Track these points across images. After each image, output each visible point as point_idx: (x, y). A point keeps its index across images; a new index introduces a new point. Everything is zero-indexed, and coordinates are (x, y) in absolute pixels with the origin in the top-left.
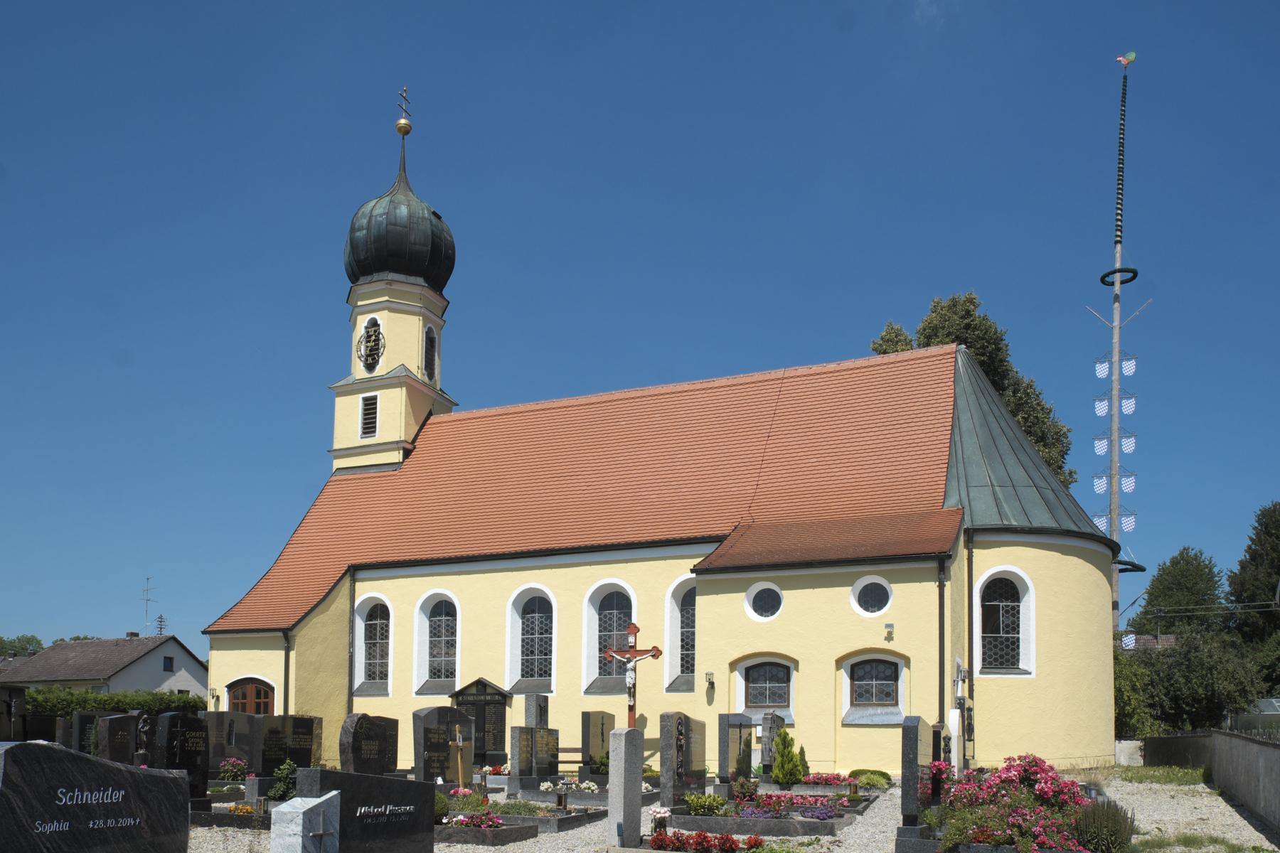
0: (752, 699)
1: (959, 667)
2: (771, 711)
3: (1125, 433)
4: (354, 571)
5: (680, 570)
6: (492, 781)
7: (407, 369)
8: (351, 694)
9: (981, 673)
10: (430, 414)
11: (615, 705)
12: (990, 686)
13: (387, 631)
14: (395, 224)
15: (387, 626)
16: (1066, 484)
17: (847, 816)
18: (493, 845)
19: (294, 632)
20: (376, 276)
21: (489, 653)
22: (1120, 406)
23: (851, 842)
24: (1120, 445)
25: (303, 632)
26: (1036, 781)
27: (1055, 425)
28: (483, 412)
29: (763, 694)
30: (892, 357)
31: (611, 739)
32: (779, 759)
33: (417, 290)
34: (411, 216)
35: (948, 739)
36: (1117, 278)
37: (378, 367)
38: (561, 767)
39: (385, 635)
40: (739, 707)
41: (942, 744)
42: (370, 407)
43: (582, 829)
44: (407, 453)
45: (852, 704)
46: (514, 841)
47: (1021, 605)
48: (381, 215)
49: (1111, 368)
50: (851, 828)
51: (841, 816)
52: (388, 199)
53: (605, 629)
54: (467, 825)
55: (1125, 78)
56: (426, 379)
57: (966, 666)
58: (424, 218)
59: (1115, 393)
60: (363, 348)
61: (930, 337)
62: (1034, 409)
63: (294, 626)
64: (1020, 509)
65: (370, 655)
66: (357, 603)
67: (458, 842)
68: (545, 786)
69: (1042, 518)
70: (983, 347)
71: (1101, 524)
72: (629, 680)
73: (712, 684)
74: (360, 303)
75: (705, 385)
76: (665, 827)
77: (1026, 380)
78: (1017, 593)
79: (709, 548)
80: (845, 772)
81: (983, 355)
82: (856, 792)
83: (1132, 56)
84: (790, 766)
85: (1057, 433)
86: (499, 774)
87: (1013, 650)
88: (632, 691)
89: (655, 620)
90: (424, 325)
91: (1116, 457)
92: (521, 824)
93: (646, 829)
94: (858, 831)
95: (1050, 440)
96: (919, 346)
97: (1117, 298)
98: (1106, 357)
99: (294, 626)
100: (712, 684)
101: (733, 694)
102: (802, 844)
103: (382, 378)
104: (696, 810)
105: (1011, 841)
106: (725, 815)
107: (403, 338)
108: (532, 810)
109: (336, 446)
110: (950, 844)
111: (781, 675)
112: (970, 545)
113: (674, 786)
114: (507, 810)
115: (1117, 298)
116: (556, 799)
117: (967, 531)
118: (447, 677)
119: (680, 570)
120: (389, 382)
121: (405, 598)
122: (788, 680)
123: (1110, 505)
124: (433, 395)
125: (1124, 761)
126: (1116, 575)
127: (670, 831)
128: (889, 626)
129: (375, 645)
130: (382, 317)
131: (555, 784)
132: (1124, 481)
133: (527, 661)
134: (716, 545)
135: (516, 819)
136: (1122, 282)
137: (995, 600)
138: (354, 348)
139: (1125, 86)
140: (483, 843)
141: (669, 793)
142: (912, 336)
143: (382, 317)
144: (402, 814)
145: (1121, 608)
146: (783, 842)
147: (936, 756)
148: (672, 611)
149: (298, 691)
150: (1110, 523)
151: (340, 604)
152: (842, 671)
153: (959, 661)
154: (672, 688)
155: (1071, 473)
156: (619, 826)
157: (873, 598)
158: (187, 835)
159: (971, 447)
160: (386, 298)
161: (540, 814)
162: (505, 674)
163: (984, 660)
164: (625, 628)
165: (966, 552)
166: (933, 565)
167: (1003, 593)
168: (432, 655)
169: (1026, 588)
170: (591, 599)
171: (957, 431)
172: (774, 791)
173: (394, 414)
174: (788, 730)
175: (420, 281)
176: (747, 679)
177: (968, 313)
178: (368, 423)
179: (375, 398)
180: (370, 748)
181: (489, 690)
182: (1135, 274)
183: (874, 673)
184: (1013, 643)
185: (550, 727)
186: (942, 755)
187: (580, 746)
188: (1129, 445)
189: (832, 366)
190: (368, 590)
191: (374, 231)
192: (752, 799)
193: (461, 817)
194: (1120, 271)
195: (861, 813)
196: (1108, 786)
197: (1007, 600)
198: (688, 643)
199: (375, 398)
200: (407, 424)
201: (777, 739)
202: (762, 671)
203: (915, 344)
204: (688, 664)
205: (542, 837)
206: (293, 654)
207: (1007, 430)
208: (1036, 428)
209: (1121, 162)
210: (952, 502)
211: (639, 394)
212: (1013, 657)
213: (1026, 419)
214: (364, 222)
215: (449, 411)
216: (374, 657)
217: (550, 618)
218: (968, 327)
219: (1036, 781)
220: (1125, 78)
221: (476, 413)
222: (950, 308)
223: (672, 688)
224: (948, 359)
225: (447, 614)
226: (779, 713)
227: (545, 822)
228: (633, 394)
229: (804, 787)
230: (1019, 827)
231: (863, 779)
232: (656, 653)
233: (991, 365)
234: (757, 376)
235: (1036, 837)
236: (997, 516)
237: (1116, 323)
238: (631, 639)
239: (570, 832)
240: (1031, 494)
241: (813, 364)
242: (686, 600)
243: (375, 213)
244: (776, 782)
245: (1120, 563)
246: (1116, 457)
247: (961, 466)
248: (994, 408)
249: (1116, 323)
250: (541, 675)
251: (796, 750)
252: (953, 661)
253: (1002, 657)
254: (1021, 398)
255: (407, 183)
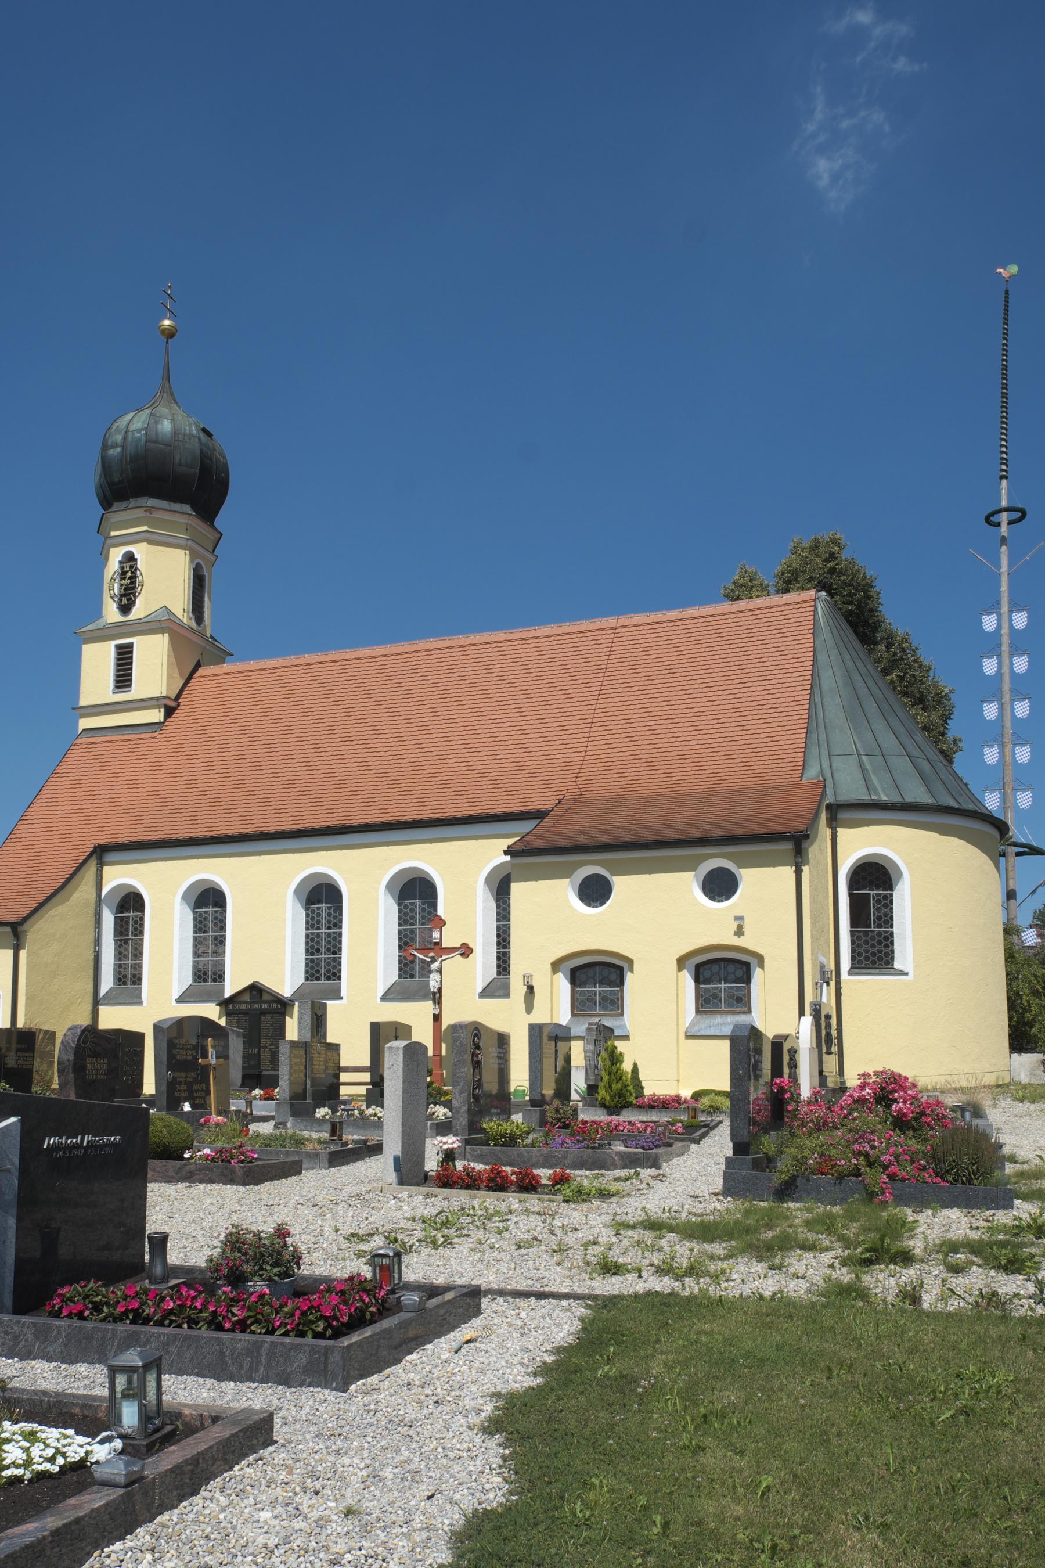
0: (579, 1006)
1: (822, 967)
2: (597, 1020)
3: (1018, 694)
4: (102, 853)
5: (491, 852)
6: (261, 1107)
7: (169, 612)
8: (96, 1003)
9: (850, 973)
10: (198, 665)
11: (417, 1017)
12: (862, 991)
13: (142, 925)
14: (156, 442)
15: (142, 919)
16: (948, 757)
17: (678, 1145)
18: (244, 1184)
19: (25, 927)
20: (133, 502)
21: (266, 952)
22: (1011, 664)
23: (677, 1175)
24: (1013, 709)
25: (36, 927)
26: (895, 1101)
27: (935, 684)
28: (263, 663)
29: (591, 1000)
30: (742, 605)
31: (386, 1054)
32: (606, 1078)
33: (182, 519)
34: (175, 432)
35: (793, 1052)
36: (1004, 517)
37: (134, 609)
38: (344, 1090)
39: (139, 931)
40: (564, 1017)
41: (786, 1058)
42: (124, 656)
43: (359, 1164)
44: (169, 712)
45: (697, 1012)
46: (271, 1179)
47: (896, 894)
48: (139, 431)
49: (999, 621)
50: (681, 1159)
51: (670, 1145)
52: (148, 411)
53: (406, 922)
54: (213, 1160)
55: (1007, 292)
56: (194, 624)
57: (832, 967)
58: (191, 435)
59: (1005, 648)
60: (116, 586)
61: (789, 582)
62: (910, 667)
63: (26, 919)
64: (890, 781)
65: (120, 955)
66: (105, 891)
67: (201, 1181)
68: (322, 1112)
69: (917, 794)
70: (850, 595)
71: (992, 802)
72: (433, 983)
73: (531, 989)
74: (113, 534)
75: (525, 635)
76: (453, 1160)
77: (901, 633)
78: (890, 879)
79: (526, 826)
80: (686, 1093)
81: (850, 603)
82: (695, 1117)
83: (1014, 269)
84: (619, 1086)
85: (937, 694)
86: (270, 1098)
87: (887, 946)
88: (437, 998)
89: (464, 910)
90: (192, 561)
91: (1008, 723)
92: (282, 1158)
93: (432, 1164)
94: (689, 1163)
95: (930, 702)
96: (778, 592)
97: (1003, 540)
98: (994, 608)
99: (26, 919)
100: (531, 989)
101: (556, 1003)
102: (618, 1179)
103: (138, 622)
104: (495, 1139)
105: (856, 1172)
106: (533, 1145)
107: (165, 575)
108: (299, 1142)
109: (83, 702)
110: (785, 1177)
111: (614, 977)
112: (833, 823)
113: (469, 1111)
114: (268, 1141)
115: (1003, 540)
116: (328, 1127)
117: (829, 807)
118: (215, 980)
119: (491, 852)
120: (147, 627)
121: (163, 886)
122: (621, 983)
123: (1005, 778)
124: (202, 643)
125: (1024, 1078)
126: (1012, 859)
127: (459, 1165)
128: (738, 918)
129: (126, 942)
130: (140, 551)
131: (334, 1110)
132: (1018, 750)
133: (312, 961)
134: (536, 822)
135: (278, 1153)
136: (1010, 523)
137: (863, 888)
138: (106, 587)
139: (1007, 301)
140: (232, 1181)
141: (463, 1121)
142: (770, 581)
143: (140, 551)
144: (105, 1145)
145: (1020, 897)
146: (596, 1177)
147: (777, 1071)
148: (485, 901)
149: (29, 998)
150: (1004, 799)
151: (83, 892)
152: (685, 971)
153: (824, 960)
154: (488, 992)
155: (955, 741)
156: (396, 1159)
157: (720, 886)
158: (146, 1187)
159: (834, 709)
160: (145, 528)
161: (310, 1147)
162: (286, 978)
163: (853, 958)
164: (430, 920)
165: (829, 831)
166: (789, 846)
167: (873, 879)
168: (196, 954)
169: (900, 874)
170: (389, 886)
171: (817, 690)
172: (600, 1116)
173: (154, 665)
174: (617, 1043)
175: (187, 508)
176: (574, 981)
177: (832, 556)
178: (122, 676)
179: (130, 646)
180: (97, 1068)
181: (265, 997)
182: (1024, 514)
183: (722, 974)
184: (886, 939)
185: (329, 1040)
186: (786, 1070)
187: (368, 1063)
188: (1022, 709)
189: (673, 614)
190: (118, 876)
191: (130, 449)
192: (566, 1126)
193: (207, 1151)
194: (1006, 510)
195: (697, 1141)
196: (995, 1106)
197: (878, 887)
198: (503, 939)
199: (130, 646)
200: (170, 677)
201: (603, 1054)
202: (590, 972)
203: (772, 589)
204: (503, 964)
205: (307, 1175)
206: (23, 954)
207: (875, 690)
208: (913, 689)
209: (1005, 386)
210: (812, 772)
211: (447, 644)
212: (887, 954)
213: (901, 678)
214: (119, 438)
215: (222, 661)
216: (126, 957)
217: (339, 909)
218: (832, 571)
219: (895, 1101)
220: (1007, 292)
221: (253, 665)
222: (811, 549)
223: (488, 992)
224: (807, 605)
225: (216, 905)
226: (608, 1022)
227: (314, 1156)
228: (441, 644)
229: (636, 1111)
230: (866, 1155)
231: (706, 1101)
232: (466, 951)
233: (859, 617)
234: (586, 625)
235: (886, 1167)
236: (865, 790)
237: (1004, 569)
238: (436, 935)
239: (344, 1168)
240: (903, 764)
241: (478, 632)
242: (501, 889)
243: (132, 428)
244: (603, 1106)
245: (1015, 845)
246: (1008, 723)
247: (822, 730)
248: (860, 665)
249: (1004, 569)
250: (328, 978)
251: (627, 1066)
252: (814, 960)
253: (873, 954)
254: (895, 654)
255: (172, 394)
